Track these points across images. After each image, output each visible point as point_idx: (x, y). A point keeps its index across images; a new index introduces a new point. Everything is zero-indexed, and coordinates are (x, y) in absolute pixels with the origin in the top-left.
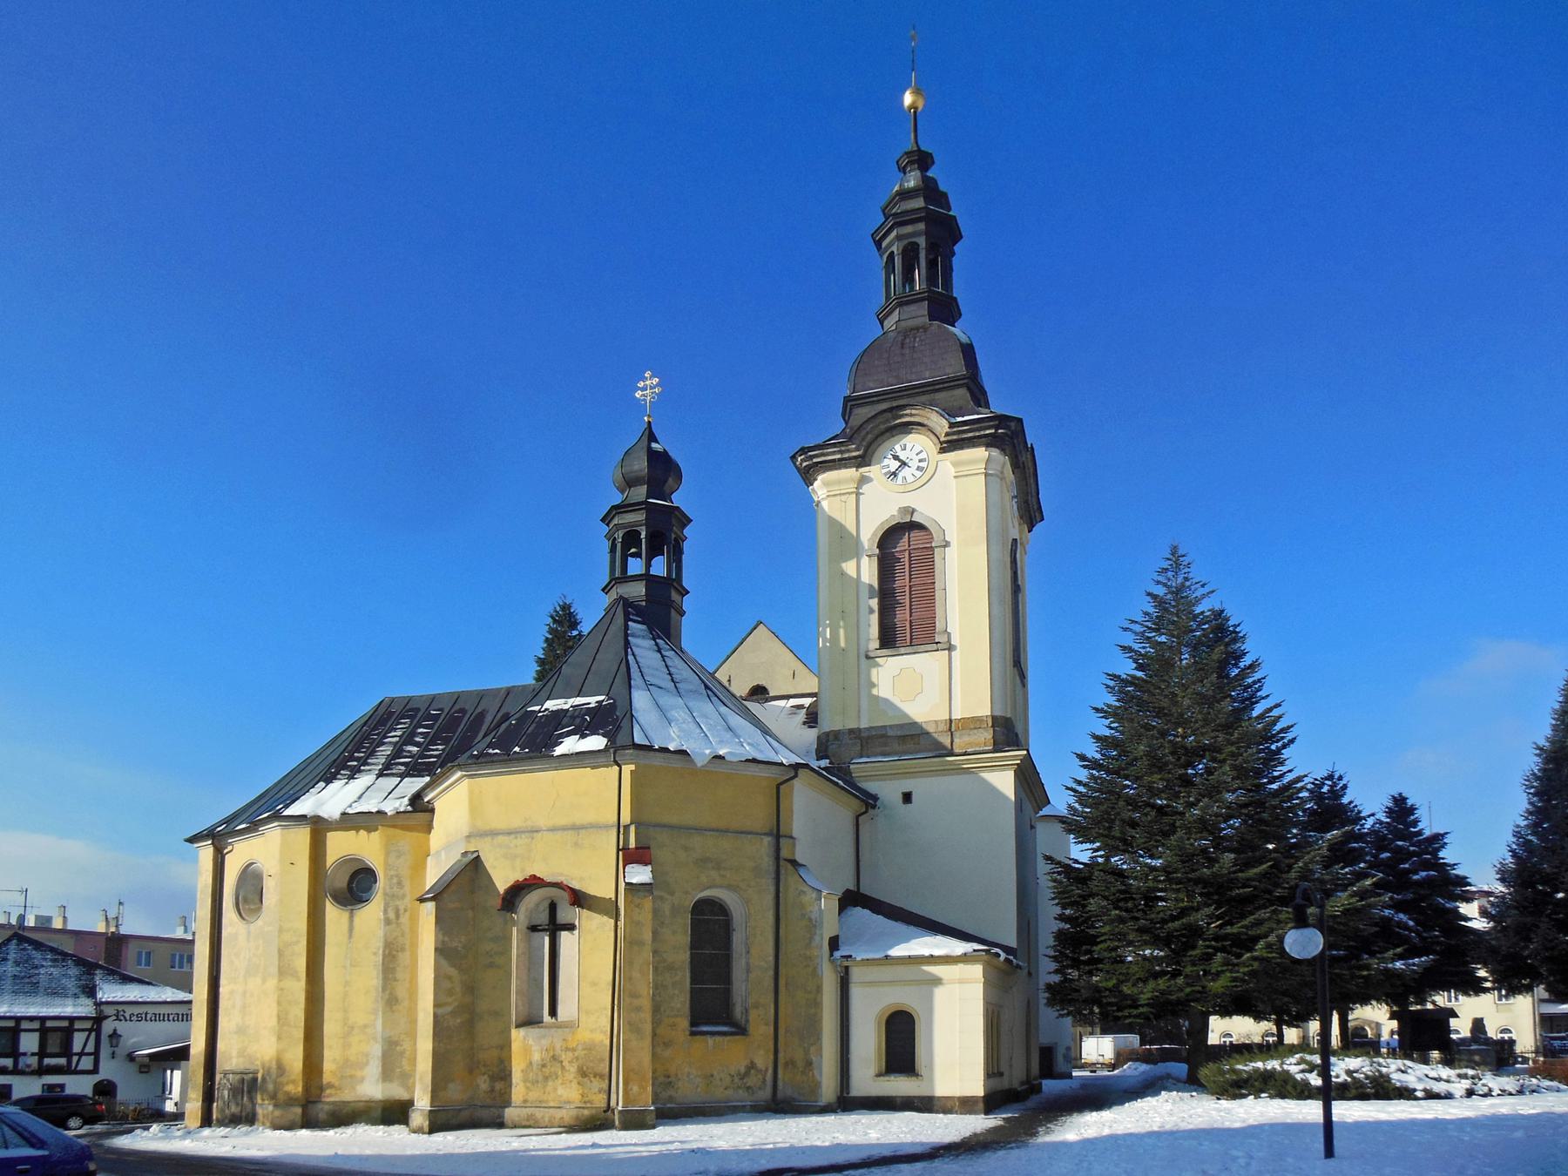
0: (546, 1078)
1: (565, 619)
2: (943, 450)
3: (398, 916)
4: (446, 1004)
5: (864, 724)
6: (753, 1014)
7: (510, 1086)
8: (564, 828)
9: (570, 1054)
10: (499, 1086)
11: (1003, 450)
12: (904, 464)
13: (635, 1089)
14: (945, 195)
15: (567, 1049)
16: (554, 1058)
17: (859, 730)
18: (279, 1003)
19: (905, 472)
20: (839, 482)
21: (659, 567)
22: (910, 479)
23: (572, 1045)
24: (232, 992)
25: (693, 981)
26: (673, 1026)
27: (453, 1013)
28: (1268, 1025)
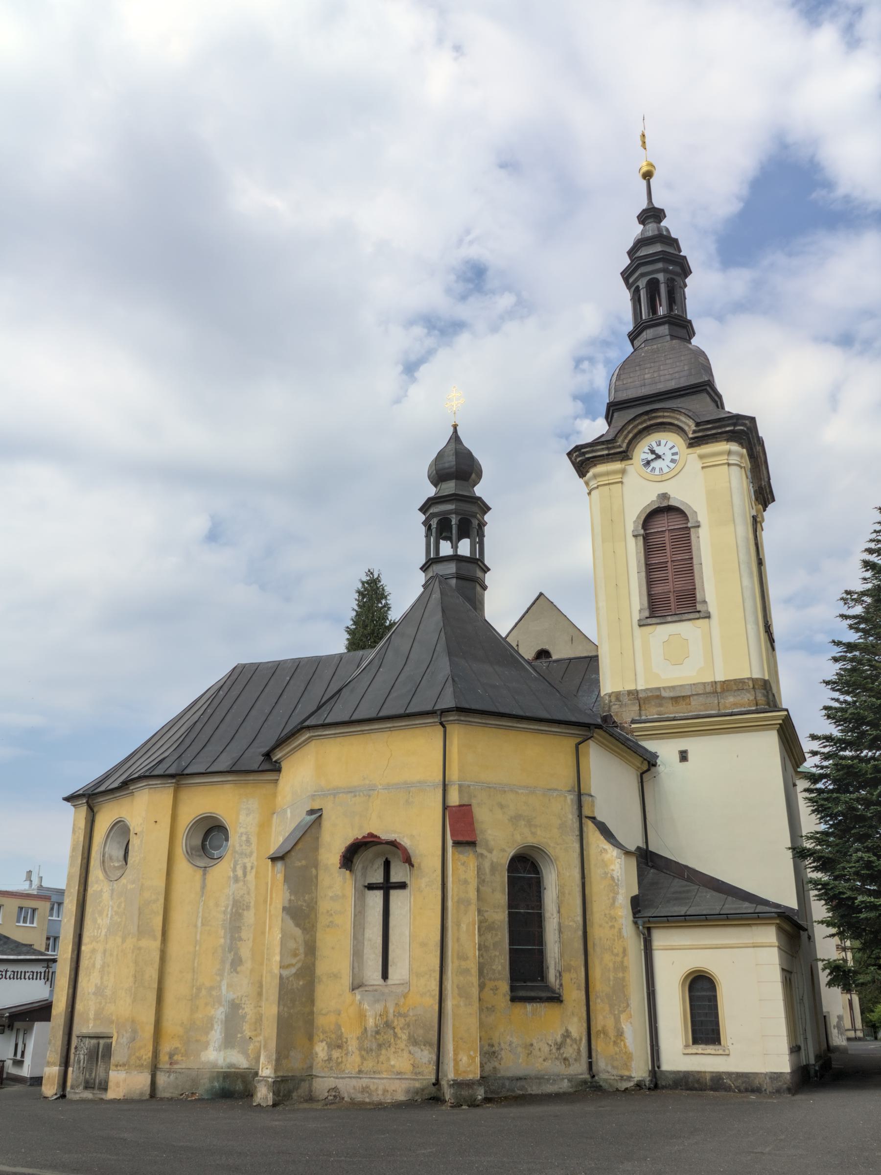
0: (380, 1046)
1: (372, 594)
3: (245, 874)
5: (641, 686)
6: (566, 977)
9: (402, 1020)
10: (336, 1054)
11: (741, 445)
12: (658, 457)
14: (676, 241)
16: (388, 1025)
17: (637, 691)
18: (136, 963)
19: (657, 464)
20: (608, 474)
21: (465, 548)
22: (666, 470)
23: (403, 1010)
24: (94, 951)
25: (511, 943)
26: (495, 989)
27: (297, 975)
28: (861, 1027)
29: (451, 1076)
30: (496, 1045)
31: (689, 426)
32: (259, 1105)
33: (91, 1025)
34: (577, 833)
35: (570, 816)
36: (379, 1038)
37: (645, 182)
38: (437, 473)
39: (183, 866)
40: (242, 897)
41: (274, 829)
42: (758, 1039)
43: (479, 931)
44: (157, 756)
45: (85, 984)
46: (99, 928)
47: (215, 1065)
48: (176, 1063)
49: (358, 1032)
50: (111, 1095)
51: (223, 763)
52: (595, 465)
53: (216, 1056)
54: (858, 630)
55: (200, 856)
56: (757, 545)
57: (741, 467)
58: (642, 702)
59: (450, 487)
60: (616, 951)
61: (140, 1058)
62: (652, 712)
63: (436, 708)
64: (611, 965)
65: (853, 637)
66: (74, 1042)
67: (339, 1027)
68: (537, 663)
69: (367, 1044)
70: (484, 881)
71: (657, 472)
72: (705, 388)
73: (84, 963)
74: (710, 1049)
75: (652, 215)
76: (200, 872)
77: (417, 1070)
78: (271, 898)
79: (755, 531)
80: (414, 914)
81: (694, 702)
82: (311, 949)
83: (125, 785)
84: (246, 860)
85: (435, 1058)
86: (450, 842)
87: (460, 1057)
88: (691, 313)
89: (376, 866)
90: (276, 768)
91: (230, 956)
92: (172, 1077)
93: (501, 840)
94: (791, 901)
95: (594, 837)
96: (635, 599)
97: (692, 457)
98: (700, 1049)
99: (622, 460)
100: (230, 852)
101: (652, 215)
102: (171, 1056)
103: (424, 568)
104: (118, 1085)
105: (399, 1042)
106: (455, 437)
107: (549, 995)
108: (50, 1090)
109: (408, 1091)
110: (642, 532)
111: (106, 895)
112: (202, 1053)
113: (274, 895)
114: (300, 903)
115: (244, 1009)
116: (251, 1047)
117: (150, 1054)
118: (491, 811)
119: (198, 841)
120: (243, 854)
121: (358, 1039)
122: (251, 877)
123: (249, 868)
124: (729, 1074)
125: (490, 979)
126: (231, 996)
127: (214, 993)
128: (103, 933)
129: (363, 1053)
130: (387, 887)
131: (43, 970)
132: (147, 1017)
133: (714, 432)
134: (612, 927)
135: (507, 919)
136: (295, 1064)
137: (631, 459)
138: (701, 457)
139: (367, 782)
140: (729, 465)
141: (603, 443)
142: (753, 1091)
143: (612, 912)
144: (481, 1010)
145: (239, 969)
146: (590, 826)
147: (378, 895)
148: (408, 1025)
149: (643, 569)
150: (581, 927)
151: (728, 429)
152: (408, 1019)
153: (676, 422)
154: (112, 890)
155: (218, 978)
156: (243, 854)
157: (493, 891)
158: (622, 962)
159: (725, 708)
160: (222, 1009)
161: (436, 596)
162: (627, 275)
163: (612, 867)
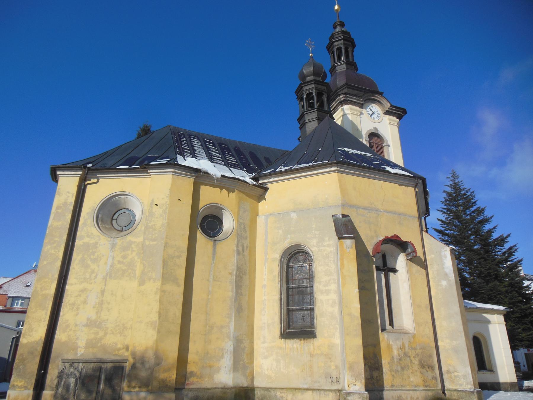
0: (403, 368)
2: (385, 113)
7: (382, 374)
8: (395, 213)
10: (375, 374)
16: (406, 354)
18: (161, 302)
39: (200, 237)
69: (395, 367)
77: (426, 384)
115: (244, 343)
121: (389, 363)
123: (245, 247)
129: (393, 373)
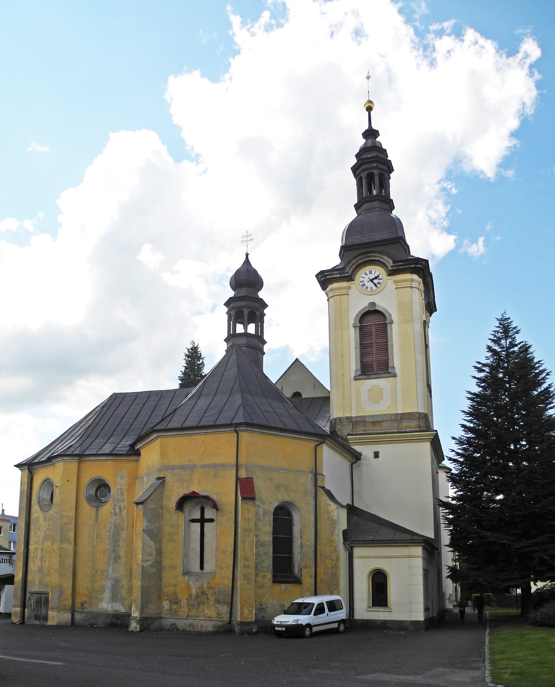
0: (199, 604)
4: (148, 561)
5: (354, 415)
6: (304, 572)
9: (211, 591)
10: (174, 607)
11: (419, 276)
12: (372, 280)
13: (246, 611)
14: (385, 151)
15: (210, 588)
16: (203, 593)
17: (351, 417)
20: (339, 289)
21: (251, 329)
24: (36, 549)
25: (274, 552)
26: (264, 577)
27: (151, 566)
29: (239, 619)
30: (264, 605)
31: (389, 263)
32: (132, 631)
33: (37, 587)
34: (314, 495)
35: (310, 486)
36: (199, 599)
37: (367, 113)
38: (235, 283)
40: (119, 523)
41: (137, 487)
42: (408, 601)
43: (256, 546)
44: (67, 444)
45: (33, 566)
46: (38, 537)
47: (107, 611)
48: (85, 608)
49: (187, 596)
50: (49, 623)
51: (107, 449)
52: (332, 283)
53: (106, 605)
54: (479, 386)
55: (94, 500)
56: (425, 336)
57: (419, 289)
58: (354, 424)
59: (244, 292)
60: (333, 558)
61: (64, 605)
62: (360, 429)
63: (233, 422)
64: (330, 565)
65: (477, 390)
66: (28, 596)
67: (176, 593)
68: (293, 400)
69: (192, 602)
70: (259, 519)
71: (369, 289)
72: (399, 241)
73: (31, 555)
74: (381, 609)
75: (371, 134)
76: (95, 509)
77: (220, 616)
78: (136, 525)
79: (425, 328)
80: (218, 535)
81: (384, 424)
82: (159, 552)
83: (50, 459)
84: (121, 504)
85: (229, 610)
86: (240, 498)
87: (244, 610)
88: (393, 195)
89: (196, 510)
90: (137, 453)
91: (113, 555)
92: (83, 615)
93: (268, 499)
94: (431, 535)
95: (323, 498)
96: (353, 364)
97: (390, 282)
98: (376, 609)
99: (348, 281)
100: (112, 499)
101: (371, 134)
102: (82, 605)
103: (226, 340)
104: (53, 618)
105: (210, 602)
106: (247, 262)
107: (294, 580)
108: (16, 619)
109: (214, 626)
110: (359, 325)
111: (41, 520)
112: (99, 604)
113: (138, 523)
114: (152, 528)
116: (127, 602)
117: (70, 603)
118: (264, 481)
119: (92, 492)
120: (119, 501)
122: (124, 513)
123: (123, 508)
124: (391, 621)
125: (262, 571)
126: (115, 575)
127: (105, 573)
128: (41, 539)
129: (190, 607)
130: (202, 521)
131: (8, 558)
132: (68, 584)
133: (404, 267)
134: (331, 546)
135: (272, 540)
136: (152, 611)
137: (354, 281)
138: (396, 282)
139: (191, 463)
140: (411, 287)
141: (337, 270)
142: (403, 630)
143: (332, 538)
144: (256, 587)
145: (118, 561)
146: (321, 492)
147: (198, 525)
148: (215, 593)
149: (359, 347)
150: (314, 545)
151: (412, 266)
152: (215, 590)
153: (381, 260)
154: (45, 517)
155: (107, 566)
156: (119, 501)
157: (265, 525)
158: (336, 564)
159: (402, 429)
160: (110, 582)
161: (234, 357)
162: (355, 169)
163: (333, 514)
